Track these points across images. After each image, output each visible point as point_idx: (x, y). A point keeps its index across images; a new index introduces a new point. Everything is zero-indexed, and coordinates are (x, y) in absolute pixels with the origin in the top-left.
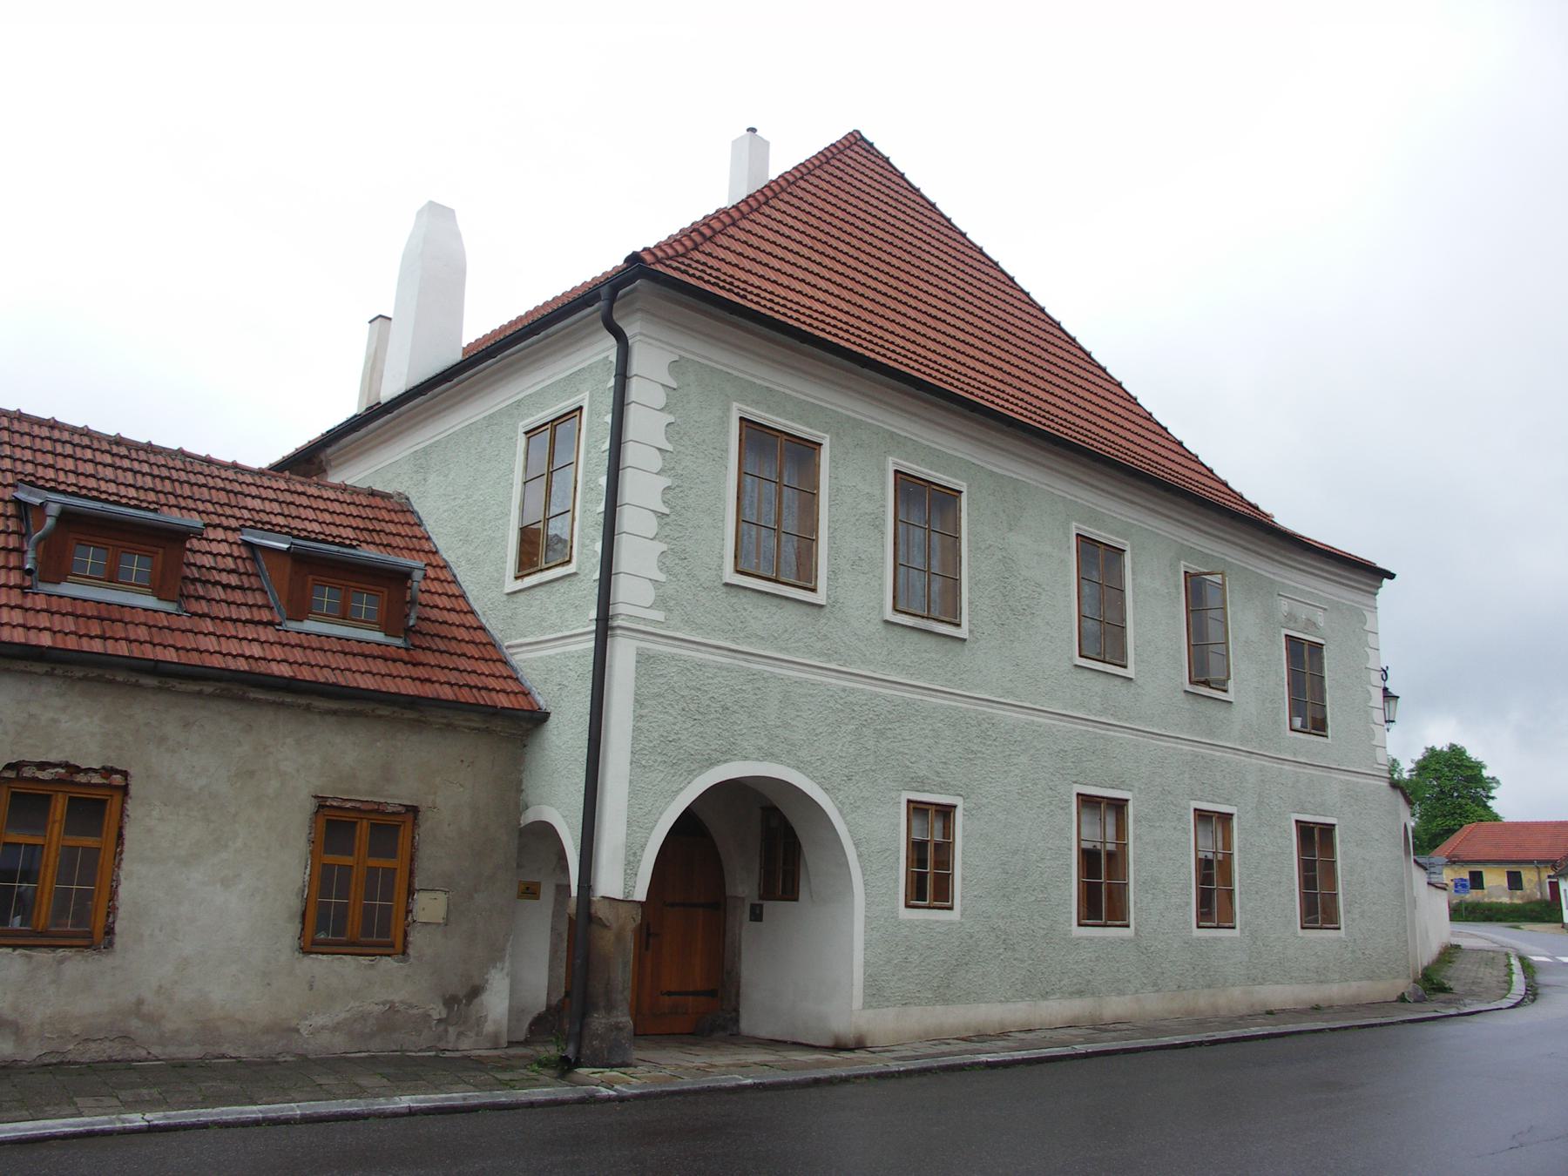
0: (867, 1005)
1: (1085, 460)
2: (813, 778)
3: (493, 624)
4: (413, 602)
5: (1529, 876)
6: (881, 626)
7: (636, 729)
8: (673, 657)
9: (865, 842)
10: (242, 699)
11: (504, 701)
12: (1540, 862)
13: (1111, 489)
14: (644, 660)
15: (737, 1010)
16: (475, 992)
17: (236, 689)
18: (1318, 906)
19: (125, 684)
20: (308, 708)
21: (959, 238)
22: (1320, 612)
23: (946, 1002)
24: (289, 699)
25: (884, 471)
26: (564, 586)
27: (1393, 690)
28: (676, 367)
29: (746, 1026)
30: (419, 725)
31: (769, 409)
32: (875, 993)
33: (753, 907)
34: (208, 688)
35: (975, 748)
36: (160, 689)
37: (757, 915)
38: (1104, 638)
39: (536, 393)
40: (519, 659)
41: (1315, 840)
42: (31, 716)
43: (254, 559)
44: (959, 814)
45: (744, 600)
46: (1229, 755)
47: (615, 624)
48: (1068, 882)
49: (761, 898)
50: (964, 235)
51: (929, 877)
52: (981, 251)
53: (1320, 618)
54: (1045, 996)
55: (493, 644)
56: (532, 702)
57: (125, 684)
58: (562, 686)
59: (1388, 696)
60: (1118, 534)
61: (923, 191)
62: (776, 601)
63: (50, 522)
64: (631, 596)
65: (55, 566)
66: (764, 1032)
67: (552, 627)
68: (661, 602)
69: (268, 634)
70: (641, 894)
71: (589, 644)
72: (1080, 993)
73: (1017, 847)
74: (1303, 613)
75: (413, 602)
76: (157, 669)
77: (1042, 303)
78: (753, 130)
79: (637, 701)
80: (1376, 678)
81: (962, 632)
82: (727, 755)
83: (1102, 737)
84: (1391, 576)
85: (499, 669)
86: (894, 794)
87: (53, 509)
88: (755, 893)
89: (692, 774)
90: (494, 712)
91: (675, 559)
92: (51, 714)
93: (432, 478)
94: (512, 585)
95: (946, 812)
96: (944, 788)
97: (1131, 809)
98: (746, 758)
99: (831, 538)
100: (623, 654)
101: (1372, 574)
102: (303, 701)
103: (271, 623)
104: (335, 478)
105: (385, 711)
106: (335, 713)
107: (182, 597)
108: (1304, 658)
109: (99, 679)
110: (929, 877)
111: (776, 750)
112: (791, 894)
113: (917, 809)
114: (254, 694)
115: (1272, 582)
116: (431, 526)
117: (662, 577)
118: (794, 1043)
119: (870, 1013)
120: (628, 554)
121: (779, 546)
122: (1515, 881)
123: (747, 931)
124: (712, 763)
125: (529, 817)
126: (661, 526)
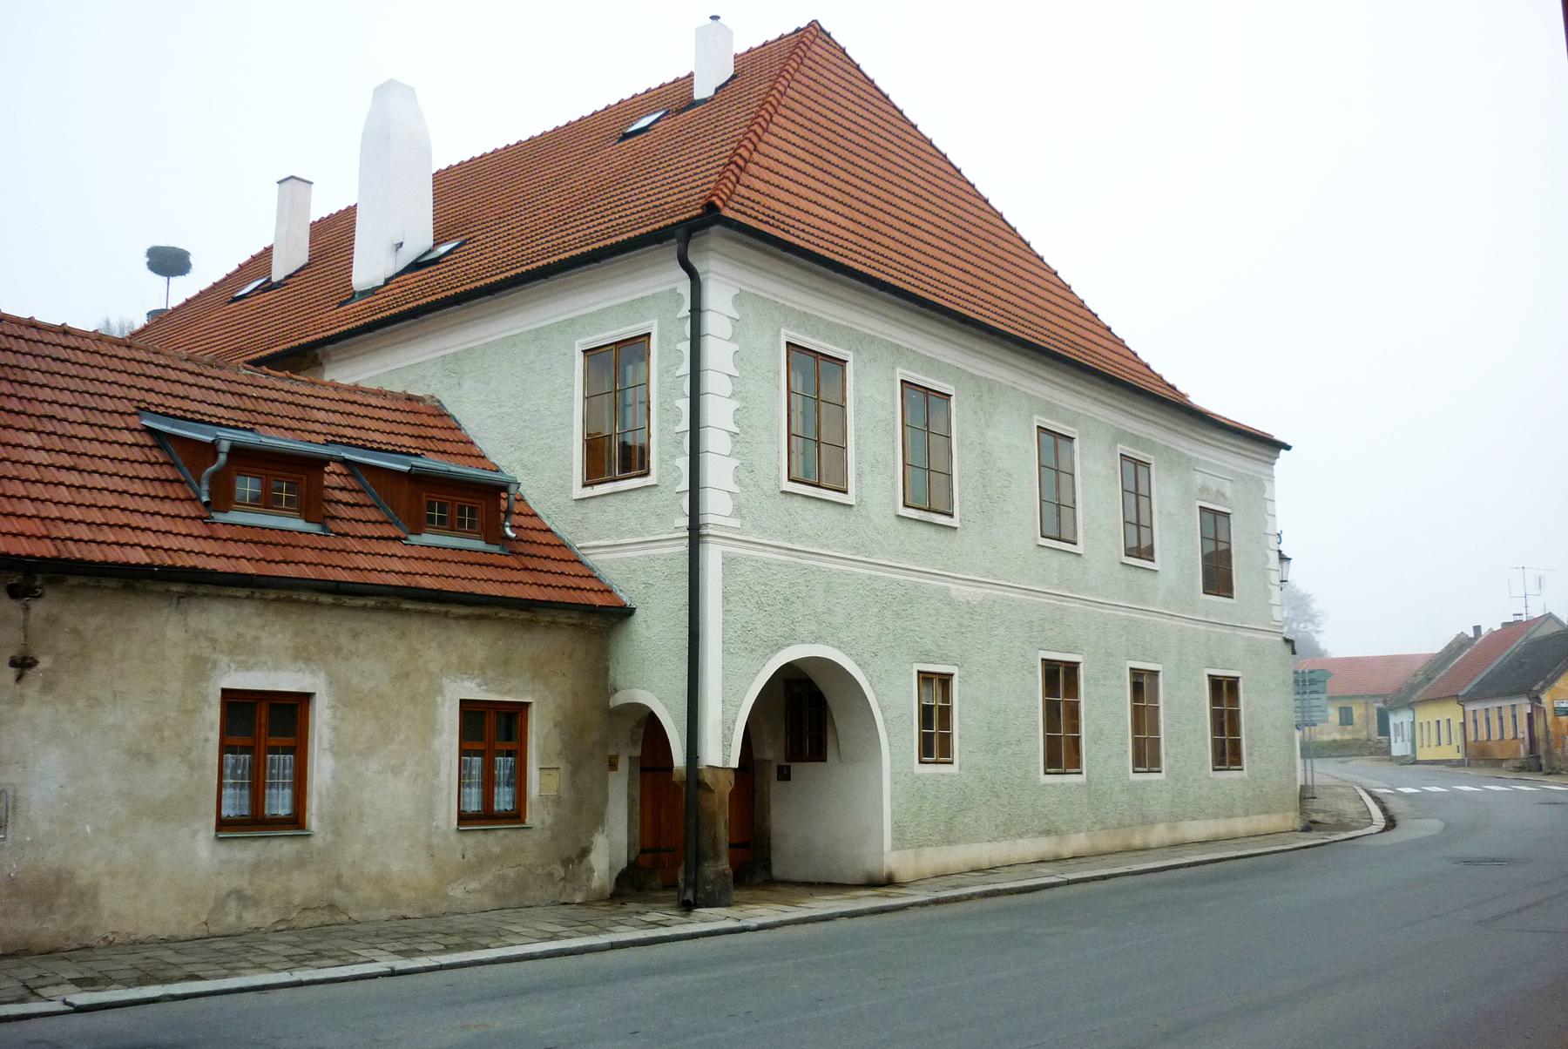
0: (894, 848)
1: (1034, 354)
2: (850, 655)
3: (562, 527)
4: (509, 512)
5: (1358, 712)
6: (894, 520)
7: (725, 622)
8: (747, 558)
9: (891, 705)
10: (396, 610)
11: (597, 600)
12: (1370, 697)
13: (1065, 383)
14: (729, 562)
15: (768, 859)
16: (584, 852)
17: (393, 602)
18: (1227, 753)
19: (307, 602)
20: (446, 615)
21: (910, 130)
22: (1228, 484)
23: (950, 842)
24: (432, 608)
25: (894, 380)
26: (643, 496)
27: (1286, 553)
28: (739, 300)
29: (777, 872)
30: (529, 625)
31: (807, 332)
32: (900, 841)
33: (780, 769)
34: (371, 602)
35: (965, 623)
36: (333, 606)
37: (784, 775)
38: (1057, 521)
39: (593, 314)
40: (594, 559)
41: (1224, 690)
42: (239, 635)
43: (352, 475)
44: (955, 682)
45: (797, 504)
46: (1156, 619)
47: (710, 531)
48: (1037, 737)
49: (787, 760)
50: (915, 127)
51: (935, 738)
52: (930, 143)
53: (1228, 489)
54: (1020, 835)
55: (562, 545)
56: (618, 599)
57: (307, 602)
58: (648, 585)
59: (1283, 558)
60: (1068, 424)
61: (877, 82)
62: (819, 504)
63: (222, 458)
64: (716, 507)
65: (223, 498)
66: (800, 874)
67: (633, 532)
68: (738, 512)
69: (396, 548)
70: (734, 763)
71: (683, 548)
72: (1047, 833)
73: (1000, 708)
74: (1213, 484)
75: (509, 512)
76: (339, 590)
77: (986, 194)
78: (715, 18)
79: (724, 598)
80: (1273, 541)
81: (954, 522)
82: (790, 639)
83: (1059, 608)
84: (1288, 448)
85: (576, 569)
86: (907, 666)
87: (225, 446)
88: (782, 755)
89: (767, 657)
90: (589, 609)
91: (746, 472)
92: (253, 633)
93: (468, 384)
94: (579, 492)
95: (945, 680)
96: (944, 659)
97: (1082, 671)
98: (803, 642)
99: (857, 444)
100: (712, 556)
101: (1278, 446)
102: (443, 609)
103: (398, 539)
104: (328, 377)
105: (504, 613)
106: (465, 617)
107: (323, 519)
108: (1215, 521)
109: (289, 600)
110: (935, 738)
111: (824, 634)
112: (819, 754)
113: (925, 678)
114: (406, 605)
115: (1189, 459)
116: (471, 428)
117: (736, 489)
118: (819, 884)
119: (895, 854)
120: (717, 471)
121: (817, 458)
122: (1346, 718)
123: (776, 787)
124: (779, 648)
125: (620, 699)
126: (735, 443)
